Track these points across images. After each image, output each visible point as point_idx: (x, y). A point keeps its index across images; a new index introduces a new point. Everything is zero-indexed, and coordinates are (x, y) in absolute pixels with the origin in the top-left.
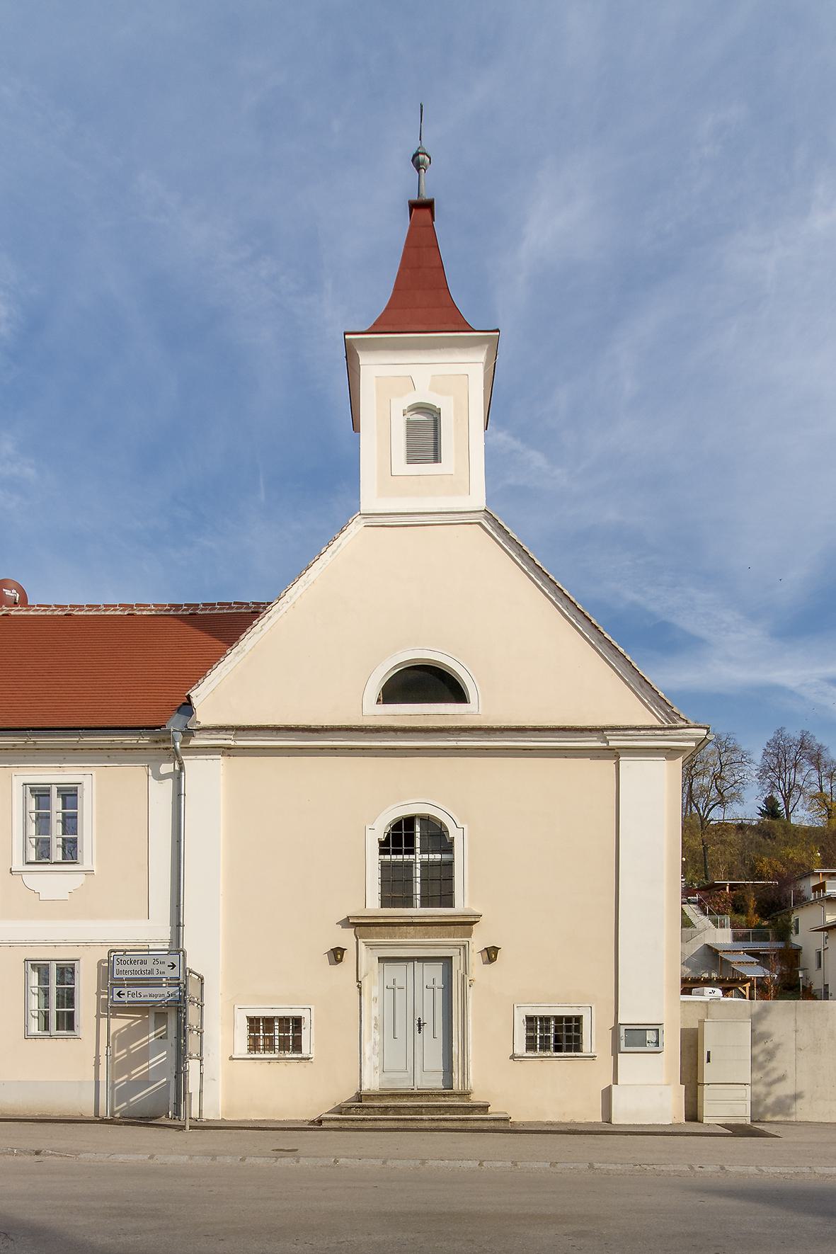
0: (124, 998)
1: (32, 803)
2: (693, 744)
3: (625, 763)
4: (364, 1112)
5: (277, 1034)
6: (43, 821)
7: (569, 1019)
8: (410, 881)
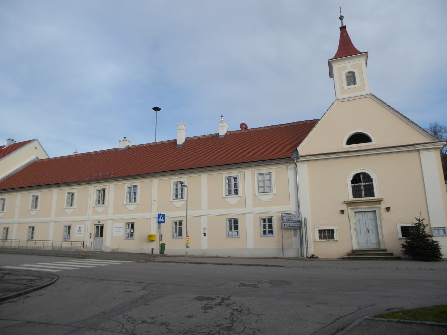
0: (286, 226)
1: (175, 186)
2: (442, 146)
3: (422, 154)
4: (355, 256)
5: (327, 234)
6: (229, 185)
7: (329, 230)
8: (361, 190)
